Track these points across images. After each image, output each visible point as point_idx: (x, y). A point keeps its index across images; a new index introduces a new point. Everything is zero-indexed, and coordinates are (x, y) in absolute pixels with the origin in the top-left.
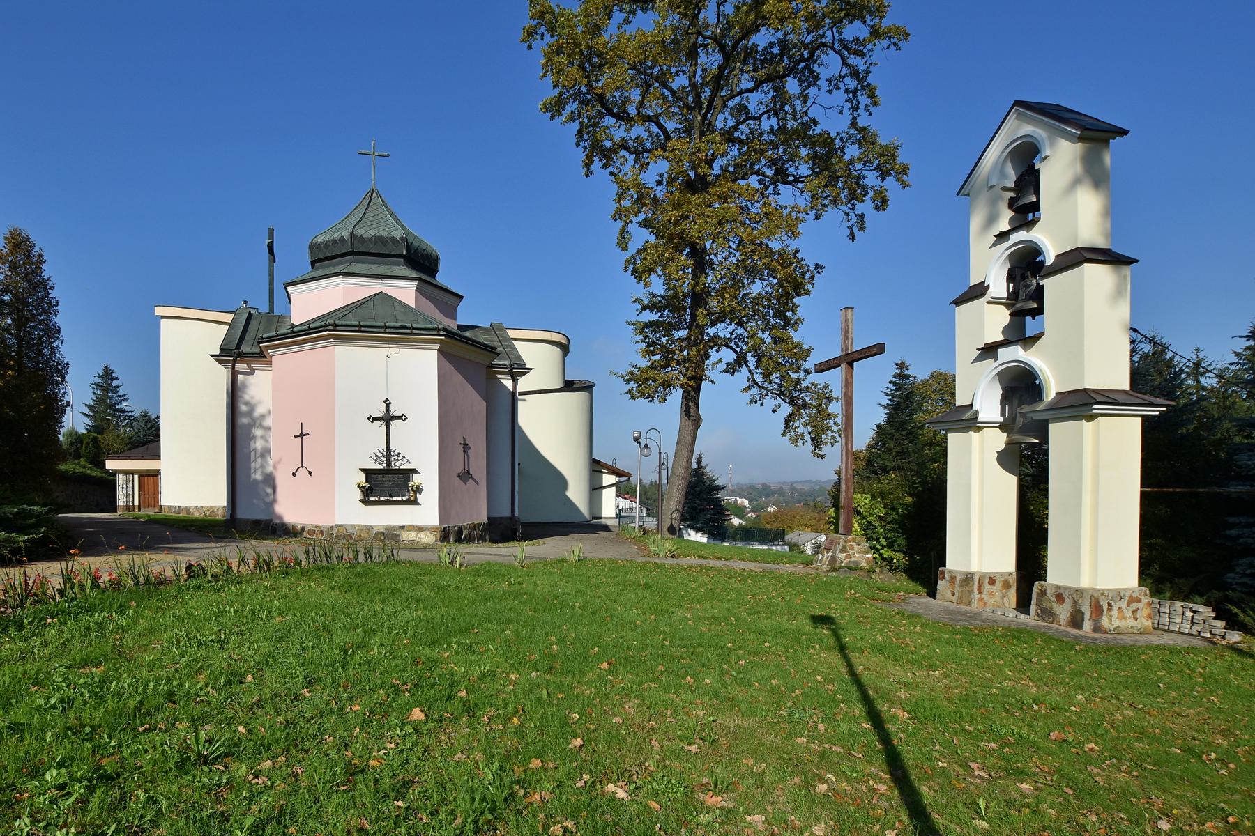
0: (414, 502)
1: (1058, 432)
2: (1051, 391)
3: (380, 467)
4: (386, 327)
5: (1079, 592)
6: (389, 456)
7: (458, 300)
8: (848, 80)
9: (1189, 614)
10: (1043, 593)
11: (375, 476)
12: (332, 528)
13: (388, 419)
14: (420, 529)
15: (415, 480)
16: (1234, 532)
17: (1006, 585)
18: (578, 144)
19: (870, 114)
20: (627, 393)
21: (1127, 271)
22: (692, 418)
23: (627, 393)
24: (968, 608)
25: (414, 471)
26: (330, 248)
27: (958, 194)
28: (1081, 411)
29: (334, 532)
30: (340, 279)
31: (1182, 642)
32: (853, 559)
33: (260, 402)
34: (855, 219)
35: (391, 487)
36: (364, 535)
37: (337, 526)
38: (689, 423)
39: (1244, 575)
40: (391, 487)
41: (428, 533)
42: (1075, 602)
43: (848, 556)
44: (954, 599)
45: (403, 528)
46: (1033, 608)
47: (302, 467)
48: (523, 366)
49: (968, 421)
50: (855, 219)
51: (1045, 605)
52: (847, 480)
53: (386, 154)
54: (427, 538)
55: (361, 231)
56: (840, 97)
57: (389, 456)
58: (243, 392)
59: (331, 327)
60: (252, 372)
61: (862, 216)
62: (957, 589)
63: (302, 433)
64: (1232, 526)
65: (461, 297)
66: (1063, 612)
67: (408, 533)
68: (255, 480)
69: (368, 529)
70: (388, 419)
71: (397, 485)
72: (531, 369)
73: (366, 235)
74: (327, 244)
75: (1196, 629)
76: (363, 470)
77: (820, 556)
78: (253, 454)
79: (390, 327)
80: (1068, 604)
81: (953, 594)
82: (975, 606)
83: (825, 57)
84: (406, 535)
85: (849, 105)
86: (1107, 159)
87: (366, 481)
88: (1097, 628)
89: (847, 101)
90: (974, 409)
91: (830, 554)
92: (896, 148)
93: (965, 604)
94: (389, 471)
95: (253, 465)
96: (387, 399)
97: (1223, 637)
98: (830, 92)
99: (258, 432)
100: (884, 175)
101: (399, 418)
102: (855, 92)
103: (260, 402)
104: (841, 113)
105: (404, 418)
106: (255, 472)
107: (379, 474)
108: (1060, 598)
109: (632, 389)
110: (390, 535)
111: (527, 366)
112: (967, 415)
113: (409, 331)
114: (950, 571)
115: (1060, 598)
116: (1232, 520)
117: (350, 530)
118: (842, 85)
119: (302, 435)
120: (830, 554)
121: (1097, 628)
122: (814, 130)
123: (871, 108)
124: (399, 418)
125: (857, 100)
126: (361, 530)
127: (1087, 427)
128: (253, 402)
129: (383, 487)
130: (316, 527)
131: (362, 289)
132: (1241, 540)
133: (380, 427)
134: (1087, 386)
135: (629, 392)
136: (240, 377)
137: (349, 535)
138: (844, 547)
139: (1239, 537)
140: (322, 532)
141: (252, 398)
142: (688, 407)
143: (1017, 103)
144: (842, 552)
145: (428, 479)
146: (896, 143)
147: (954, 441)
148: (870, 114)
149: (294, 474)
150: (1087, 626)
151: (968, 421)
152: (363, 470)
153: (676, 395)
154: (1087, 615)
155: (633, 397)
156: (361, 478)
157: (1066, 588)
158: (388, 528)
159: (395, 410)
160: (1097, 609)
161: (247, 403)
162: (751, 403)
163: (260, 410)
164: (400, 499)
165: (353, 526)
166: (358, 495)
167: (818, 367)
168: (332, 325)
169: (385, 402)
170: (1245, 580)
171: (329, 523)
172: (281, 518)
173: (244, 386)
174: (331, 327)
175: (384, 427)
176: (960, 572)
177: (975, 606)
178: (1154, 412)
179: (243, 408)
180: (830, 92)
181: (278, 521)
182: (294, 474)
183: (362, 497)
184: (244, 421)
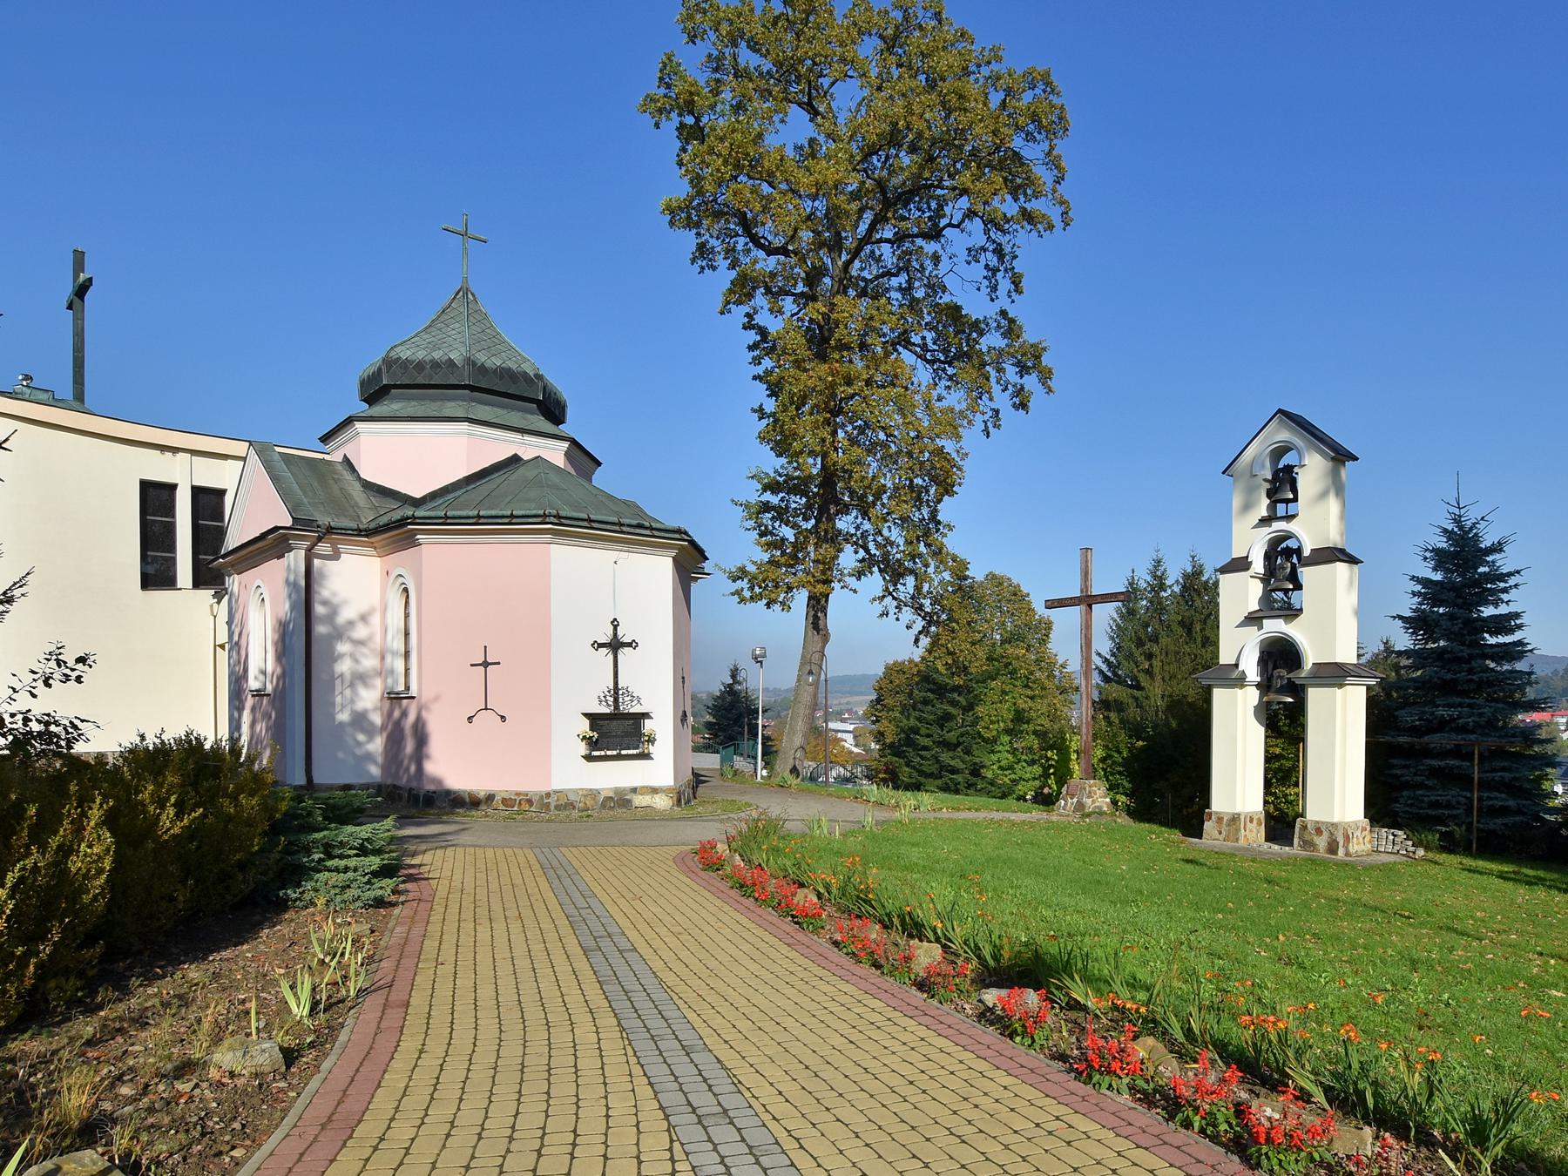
0: (646, 756)
1: (1315, 696)
2: (1311, 657)
3: (607, 711)
4: (623, 525)
5: (1334, 825)
6: (616, 700)
7: (595, 465)
8: (989, 255)
9: (1391, 837)
10: (1304, 827)
11: (601, 723)
12: (548, 795)
13: (615, 645)
14: (655, 791)
15: (648, 726)
16: (1399, 772)
17: (1259, 824)
18: (693, 261)
19: (1013, 302)
20: (733, 594)
21: (1356, 568)
22: (821, 632)
23: (733, 594)
24: (1236, 844)
25: (646, 715)
26: (426, 372)
27: (1223, 473)
28: (1338, 681)
29: (553, 801)
30: (464, 426)
31: (1392, 858)
32: (1097, 804)
33: (346, 602)
34: (990, 414)
35: (619, 736)
36: (589, 803)
37: (556, 792)
38: (817, 638)
39: (1406, 805)
40: (619, 736)
41: (664, 797)
42: (1332, 834)
43: (1093, 802)
44: (1221, 838)
45: (634, 790)
46: (1296, 840)
47: (486, 709)
48: (701, 571)
49: (1233, 678)
50: (990, 414)
51: (1306, 838)
52: (1087, 722)
53: (484, 238)
54: (662, 802)
55: (481, 358)
56: (978, 271)
57: (616, 700)
58: (320, 585)
59: (552, 519)
60: (336, 556)
61: (997, 412)
62: (1224, 829)
63: (485, 661)
64: (1394, 766)
65: (599, 464)
66: (1322, 842)
67: (641, 797)
68: (341, 724)
69: (593, 794)
70: (615, 645)
71: (627, 734)
72: (708, 574)
73: (488, 364)
74: (420, 366)
75: (1397, 848)
76: (586, 715)
77: (1063, 802)
78: (338, 682)
79: (629, 526)
80: (1326, 835)
81: (1220, 833)
82: (1242, 842)
83: (969, 224)
84: (639, 800)
85: (986, 283)
86: (1344, 473)
87: (592, 729)
88: (1347, 854)
89: (985, 277)
90: (1240, 668)
91: (1075, 800)
92: (1044, 349)
93: (1233, 841)
94: (617, 716)
95: (338, 699)
96: (615, 619)
97: (1414, 853)
98: (969, 263)
99: (343, 648)
100: (1023, 370)
101: (629, 645)
102: (995, 271)
103: (346, 602)
104: (979, 289)
105: (634, 644)
106: (341, 710)
107: (607, 719)
108: (1319, 831)
109: (742, 589)
110: (620, 800)
111: (706, 571)
112: (1235, 675)
113: (648, 532)
114: (1216, 813)
115: (1319, 831)
116: (1395, 762)
117: (572, 797)
118: (982, 259)
119: (486, 664)
120: (1075, 800)
121: (1347, 854)
122: (941, 297)
123: (1013, 294)
124: (629, 645)
125: (996, 281)
126: (585, 796)
127: (1338, 692)
128: (335, 600)
129: (609, 737)
130: (518, 794)
131: (493, 446)
132: (1403, 779)
133: (605, 656)
134: (1338, 660)
135: (738, 593)
136: (316, 562)
137: (572, 804)
138: (1090, 792)
139: (1402, 775)
140: (530, 802)
141: (335, 594)
142: (816, 618)
143: (1280, 411)
144: (1089, 797)
145: (662, 726)
146: (1044, 345)
147: (1219, 695)
148: (1013, 302)
149: (470, 719)
150: (1341, 852)
151: (1233, 678)
152: (586, 715)
153: (801, 598)
154: (1341, 844)
155: (742, 600)
156: (584, 726)
157: (1323, 823)
158: (617, 791)
159: (625, 634)
160: (1347, 839)
161: (325, 603)
162: (881, 615)
163: (346, 614)
164: (635, 752)
165: (575, 791)
166: (582, 748)
167: (1049, 603)
168: (554, 517)
169: (612, 622)
170: (1407, 809)
171: (543, 788)
172: (439, 782)
173: (322, 576)
174: (552, 519)
175: (611, 657)
176: (1227, 813)
177: (1242, 842)
178: (1372, 682)
179: (319, 610)
180: (969, 263)
181: (431, 787)
182: (470, 719)
183: (588, 752)
184: (320, 629)
